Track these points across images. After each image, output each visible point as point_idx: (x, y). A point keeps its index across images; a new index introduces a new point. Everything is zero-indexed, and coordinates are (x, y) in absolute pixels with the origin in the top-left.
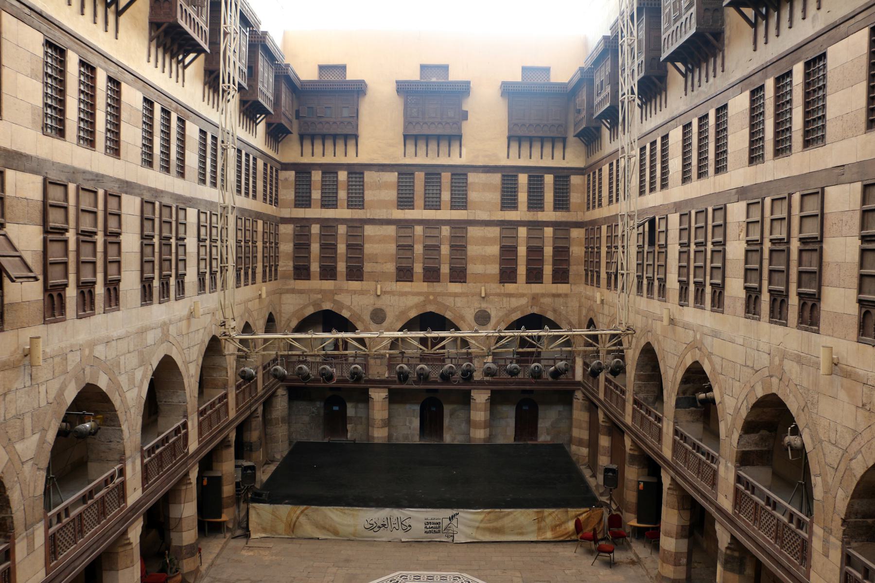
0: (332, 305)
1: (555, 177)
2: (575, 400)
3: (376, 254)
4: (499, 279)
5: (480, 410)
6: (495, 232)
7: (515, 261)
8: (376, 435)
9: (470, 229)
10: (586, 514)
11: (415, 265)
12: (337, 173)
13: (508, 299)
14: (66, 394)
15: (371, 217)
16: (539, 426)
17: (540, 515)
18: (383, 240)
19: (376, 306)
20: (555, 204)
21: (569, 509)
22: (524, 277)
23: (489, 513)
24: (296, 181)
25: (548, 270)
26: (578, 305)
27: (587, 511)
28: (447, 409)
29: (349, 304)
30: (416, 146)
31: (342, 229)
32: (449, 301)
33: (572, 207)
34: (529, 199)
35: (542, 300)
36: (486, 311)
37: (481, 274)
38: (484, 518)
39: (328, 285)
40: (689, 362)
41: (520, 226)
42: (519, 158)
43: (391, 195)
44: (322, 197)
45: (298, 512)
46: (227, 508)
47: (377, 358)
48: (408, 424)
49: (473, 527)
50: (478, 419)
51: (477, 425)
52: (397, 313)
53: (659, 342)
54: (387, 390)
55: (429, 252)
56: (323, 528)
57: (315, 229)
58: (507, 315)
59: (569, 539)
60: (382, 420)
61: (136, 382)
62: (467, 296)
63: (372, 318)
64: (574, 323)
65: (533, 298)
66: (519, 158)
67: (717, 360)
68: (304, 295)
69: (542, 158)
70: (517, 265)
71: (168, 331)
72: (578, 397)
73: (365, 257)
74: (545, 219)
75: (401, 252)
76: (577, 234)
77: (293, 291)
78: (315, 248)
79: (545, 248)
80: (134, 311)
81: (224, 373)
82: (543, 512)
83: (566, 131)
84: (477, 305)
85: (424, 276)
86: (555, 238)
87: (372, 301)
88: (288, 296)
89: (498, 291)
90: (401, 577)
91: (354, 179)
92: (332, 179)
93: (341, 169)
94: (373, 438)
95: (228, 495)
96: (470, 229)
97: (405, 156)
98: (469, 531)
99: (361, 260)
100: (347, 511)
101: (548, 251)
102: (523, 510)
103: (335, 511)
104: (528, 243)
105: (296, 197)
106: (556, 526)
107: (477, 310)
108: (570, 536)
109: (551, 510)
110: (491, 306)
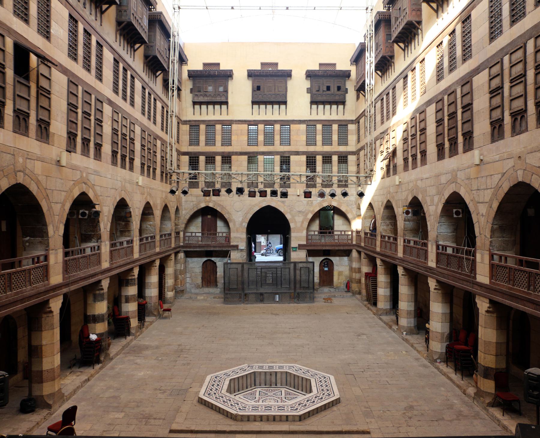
14: (409, 198)
40: (76, 193)
53: (38, 183)
61: (434, 203)
67: (97, 188)
71: (457, 175)
80: (434, 164)
90: (297, 409)
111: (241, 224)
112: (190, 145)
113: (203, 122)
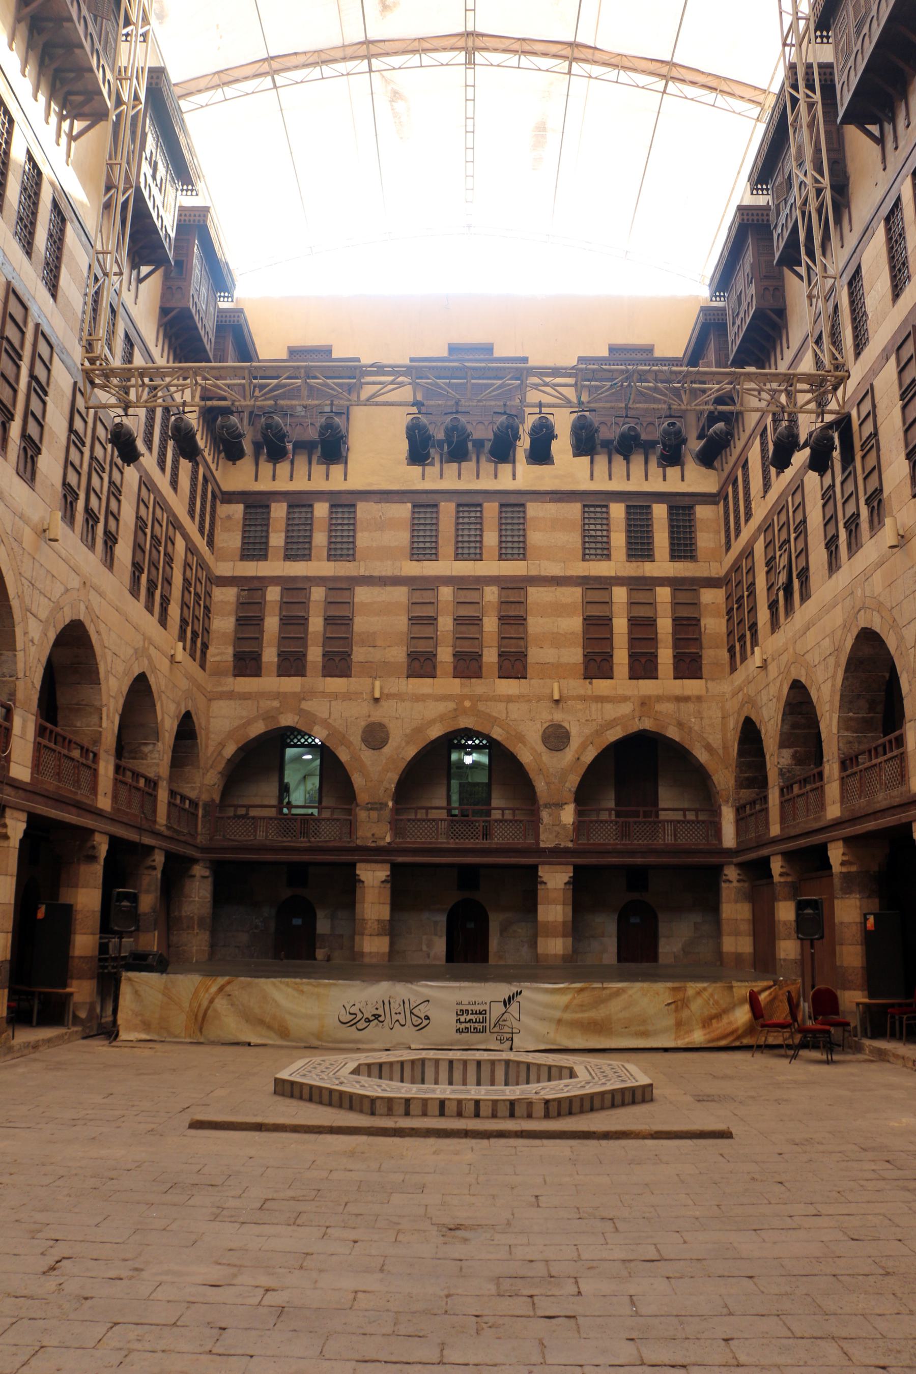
0: (297, 718)
1: (671, 508)
2: (724, 885)
3: (375, 633)
4: (582, 671)
6: (574, 594)
7: (610, 640)
8: (367, 948)
9: (531, 590)
10: (767, 993)
11: (439, 649)
12: (311, 506)
13: (600, 705)
15: (367, 574)
16: (660, 950)
17: (680, 996)
19: (372, 719)
20: (672, 550)
21: (735, 984)
23: (582, 990)
24: (245, 519)
25: (665, 656)
26: (720, 715)
27: (769, 988)
28: (495, 922)
31: (318, 594)
32: (497, 710)
33: (700, 553)
34: (629, 543)
36: (560, 726)
37: (553, 664)
38: (570, 1003)
39: (292, 684)
42: (610, 479)
43: (403, 538)
44: (287, 543)
45: (214, 989)
46: (79, 978)
47: (371, 809)
48: (424, 948)
50: (551, 918)
51: (550, 931)
52: (408, 731)
54: (388, 866)
55: (463, 628)
56: (259, 1022)
57: (273, 594)
58: (598, 733)
59: (737, 1044)
60: (378, 921)
62: (529, 701)
63: (365, 740)
64: (715, 746)
65: (643, 704)
66: (610, 479)
68: (250, 702)
69: (647, 479)
70: (612, 648)
74: (656, 574)
75: (416, 628)
76: (712, 597)
77: (231, 695)
78: (272, 624)
81: (95, 719)
84: (547, 715)
85: (455, 668)
86: (675, 604)
88: (222, 703)
89: (582, 692)
91: (340, 515)
92: (303, 515)
93: (319, 500)
94: (362, 954)
95: (82, 954)
96: (531, 590)
98: (542, 1028)
99: (348, 641)
100: (306, 988)
101: (665, 625)
102: (645, 985)
103: (283, 987)
104: (629, 611)
105: (243, 544)
107: (545, 725)
108: (738, 1038)
109: (700, 985)
111: (222, 745)
113: (660, 497)
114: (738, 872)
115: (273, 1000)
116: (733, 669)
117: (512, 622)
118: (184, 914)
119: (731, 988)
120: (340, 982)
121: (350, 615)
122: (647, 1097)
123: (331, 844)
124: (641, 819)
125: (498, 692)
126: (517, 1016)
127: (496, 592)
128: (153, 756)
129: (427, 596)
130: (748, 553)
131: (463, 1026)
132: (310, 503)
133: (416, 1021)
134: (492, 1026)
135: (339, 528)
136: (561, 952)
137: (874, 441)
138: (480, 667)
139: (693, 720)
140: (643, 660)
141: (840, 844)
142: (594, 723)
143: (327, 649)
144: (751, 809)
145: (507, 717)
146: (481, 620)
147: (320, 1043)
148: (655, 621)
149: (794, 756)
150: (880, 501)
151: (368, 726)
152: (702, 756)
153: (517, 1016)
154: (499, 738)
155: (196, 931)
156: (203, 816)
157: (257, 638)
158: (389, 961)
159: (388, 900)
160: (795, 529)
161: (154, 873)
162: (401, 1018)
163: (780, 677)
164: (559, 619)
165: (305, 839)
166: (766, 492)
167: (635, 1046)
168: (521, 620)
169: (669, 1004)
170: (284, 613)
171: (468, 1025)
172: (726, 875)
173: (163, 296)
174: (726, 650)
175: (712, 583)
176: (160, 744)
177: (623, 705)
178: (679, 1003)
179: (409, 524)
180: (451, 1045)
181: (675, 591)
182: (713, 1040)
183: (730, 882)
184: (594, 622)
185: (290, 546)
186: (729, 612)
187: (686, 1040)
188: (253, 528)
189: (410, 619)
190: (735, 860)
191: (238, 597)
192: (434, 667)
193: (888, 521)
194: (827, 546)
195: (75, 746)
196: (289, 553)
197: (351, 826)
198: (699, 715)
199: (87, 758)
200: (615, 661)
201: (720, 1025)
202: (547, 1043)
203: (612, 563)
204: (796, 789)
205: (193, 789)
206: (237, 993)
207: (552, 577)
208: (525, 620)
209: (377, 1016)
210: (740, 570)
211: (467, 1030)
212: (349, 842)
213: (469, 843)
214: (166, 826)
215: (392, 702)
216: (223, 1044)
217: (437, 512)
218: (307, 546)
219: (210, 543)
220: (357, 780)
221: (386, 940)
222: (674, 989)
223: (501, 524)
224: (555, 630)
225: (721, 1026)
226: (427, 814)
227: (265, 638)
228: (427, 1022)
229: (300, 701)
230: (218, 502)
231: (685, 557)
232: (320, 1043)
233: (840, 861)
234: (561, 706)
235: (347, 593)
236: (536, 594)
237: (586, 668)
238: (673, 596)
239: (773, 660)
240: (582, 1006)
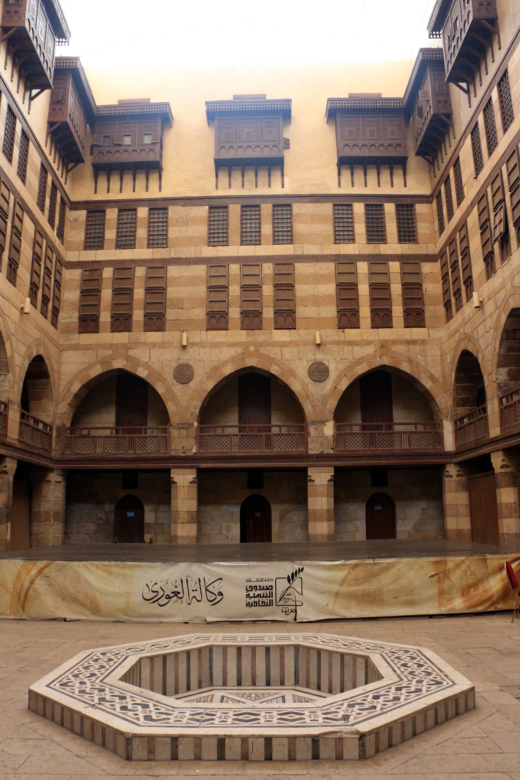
0: (125, 362)
1: (397, 206)
2: (446, 479)
3: (182, 299)
4: (337, 323)
5: (320, 495)
6: (329, 268)
7: (356, 299)
9: (297, 265)
11: (230, 309)
12: (135, 210)
13: (350, 347)
15: (176, 256)
17: (441, 568)
18: (190, 281)
19: (181, 362)
20: (399, 236)
21: (488, 556)
22: (369, 321)
23: (356, 566)
24: (87, 221)
26: (439, 354)
28: (276, 511)
29: (146, 360)
30: (230, 176)
31: (140, 272)
32: (274, 352)
33: (420, 238)
34: (368, 231)
35: (394, 348)
36: (322, 364)
37: (315, 318)
38: (346, 576)
39: (122, 337)
41: (360, 260)
42: (353, 186)
43: (202, 230)
44: (118, 237)
45: (34, 572)
47: (181, 428)
48: (224, 532)
49: (329, 593)
50: (318, 507)
52: (208, 370)
54: (195, 471)
57: (108, 273)
58: (350, 368)
59: (492, 609)
60: (188, 512)
62: (298, 345)
63: (176, 377)
64: (436, 376)
65: (382, 346)
66: (353, 186)
68: (90, 351)
69: (379, 186)
70: (358, 306)
72: (451, 473)
73: (168, 302)
75: (213, 294)
77: (77, 347)
78: (107, 294)
79: (391, 285)
82: (445, 562)
83: (405, 149)
85: (242, 322)
86: (404, 274)
87: (176, 356)
88: (70, 353)
89: (337, 338)
94: (176, 537)
96: (297, 265)
97: (217, 189)
98: (322, 600)
99: (162, 304)
100: (114, 570)
101: (396, 289)
102: (411, 560)
103: (94, 569)
104: (370, 279)
105: (86, 238)
106: (469, 587)
108: (493, 604)
109: (459, 559)
110: (328, 357)
112: (336, 241)
113: (389, 198)
114: (458, 469)
115: (86, 580)
116: (449, 317)
117: (284, 288)
118: (42, 510)
119: (485, 560)
120: (143, 563)
121: (164, 286)
122: (470, 705)
123: (151, 455)
124: (383, 431)
125: (274, 340)
126: (300, 590)
127: (272, 267)
128: (5, 384)
129: (221, 271)
130: (463, 226)
131: (252, 600)
132: (134, 208)
133: (211, 597)
134: (278, 599)
135: (156, 224)
136: (327, 533)
137: (503, 204)
138: (261, 322)
139: (420, 357)
140: (381, 314)
141: (501, 453)
142: (347, 360)
143: (147, 311)
144: (460, 424)
145: (282, 358)
146: (261, 287)
147: (127, 618)
148: (389, 286)
149: (509, 374)
150: (492, 258)
151: (178, 367)
152: (428, 384)
153: (300, 590)
154: (276, 373)
155: (52, 522)
156: (57, 437)
157: (96, 305)
158: (197, 542)
159: (195, 496)
160: (451, 266)
161: (6, 476)
162: (197, 594)
163: (497, 311)
164: (319, 286)
165: (133, 452)
166: (477, 174)
167: (404, 614)
168: (290, 287)
169: (432, 576)
170: (116, 286)
171: (256, 599)
172: (448, 472)
173: (50, 114)
174: (443, 305)
175: (429, 258)
176: (10, 375)
177: (367, 347)
178: (441, 575)
179: (207, 220)
180: (243, 617)
181: (403, 264)
182: (471, 607)
183: (451, 476)
184: (344, 287)
185: (120, 239)
186: (445, 277)
187: (449, 607)
188: (93, 227)
189: (208, 288)
190: (454, 460)
191: (82, 276)
192: (227, 322)
193: (475, 294)
194: (485, 259)
195: (31, 418)
196: (119, 243)
197: (167, 441)
198: (424, 354)
199: (46, 429)
200: (360, 316)
201: (477, 592)
202: (327, 614)
203: (356, 245)
204: (466, 421)
205: (48, 416)
206: (54, 574)
207: (312, 255)
208: (293, 286)
209: (176, 594)
210: (454, 243)
211: (256, 604)
212: (165, 453)
213: (256, 452)
214: (18, 440)
215: (195, 349)
216: (42, 620)
217: (227, 212)
218: (132, 238)
219: (61, 235)
220: (171, 407)
221: (194, 526)
222: (436, 563)
223: (274, 219)
224: (316, 294)
225: (477, 594)
226: (223, 431)
227: (102, 304)
228: (221, 597)
229: (127, 350)
230: (67, 209)
231: (410, 241)
232: (127, 618)
233: (500, 465)
234: (321, 349)
235: (161, 270)
236: (301, 268)
237: (339, 321)
238: (402, 268)
239: (490, 299)
240: (357, 580)
